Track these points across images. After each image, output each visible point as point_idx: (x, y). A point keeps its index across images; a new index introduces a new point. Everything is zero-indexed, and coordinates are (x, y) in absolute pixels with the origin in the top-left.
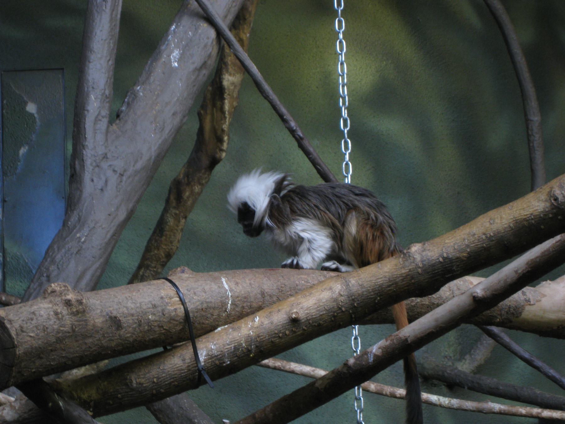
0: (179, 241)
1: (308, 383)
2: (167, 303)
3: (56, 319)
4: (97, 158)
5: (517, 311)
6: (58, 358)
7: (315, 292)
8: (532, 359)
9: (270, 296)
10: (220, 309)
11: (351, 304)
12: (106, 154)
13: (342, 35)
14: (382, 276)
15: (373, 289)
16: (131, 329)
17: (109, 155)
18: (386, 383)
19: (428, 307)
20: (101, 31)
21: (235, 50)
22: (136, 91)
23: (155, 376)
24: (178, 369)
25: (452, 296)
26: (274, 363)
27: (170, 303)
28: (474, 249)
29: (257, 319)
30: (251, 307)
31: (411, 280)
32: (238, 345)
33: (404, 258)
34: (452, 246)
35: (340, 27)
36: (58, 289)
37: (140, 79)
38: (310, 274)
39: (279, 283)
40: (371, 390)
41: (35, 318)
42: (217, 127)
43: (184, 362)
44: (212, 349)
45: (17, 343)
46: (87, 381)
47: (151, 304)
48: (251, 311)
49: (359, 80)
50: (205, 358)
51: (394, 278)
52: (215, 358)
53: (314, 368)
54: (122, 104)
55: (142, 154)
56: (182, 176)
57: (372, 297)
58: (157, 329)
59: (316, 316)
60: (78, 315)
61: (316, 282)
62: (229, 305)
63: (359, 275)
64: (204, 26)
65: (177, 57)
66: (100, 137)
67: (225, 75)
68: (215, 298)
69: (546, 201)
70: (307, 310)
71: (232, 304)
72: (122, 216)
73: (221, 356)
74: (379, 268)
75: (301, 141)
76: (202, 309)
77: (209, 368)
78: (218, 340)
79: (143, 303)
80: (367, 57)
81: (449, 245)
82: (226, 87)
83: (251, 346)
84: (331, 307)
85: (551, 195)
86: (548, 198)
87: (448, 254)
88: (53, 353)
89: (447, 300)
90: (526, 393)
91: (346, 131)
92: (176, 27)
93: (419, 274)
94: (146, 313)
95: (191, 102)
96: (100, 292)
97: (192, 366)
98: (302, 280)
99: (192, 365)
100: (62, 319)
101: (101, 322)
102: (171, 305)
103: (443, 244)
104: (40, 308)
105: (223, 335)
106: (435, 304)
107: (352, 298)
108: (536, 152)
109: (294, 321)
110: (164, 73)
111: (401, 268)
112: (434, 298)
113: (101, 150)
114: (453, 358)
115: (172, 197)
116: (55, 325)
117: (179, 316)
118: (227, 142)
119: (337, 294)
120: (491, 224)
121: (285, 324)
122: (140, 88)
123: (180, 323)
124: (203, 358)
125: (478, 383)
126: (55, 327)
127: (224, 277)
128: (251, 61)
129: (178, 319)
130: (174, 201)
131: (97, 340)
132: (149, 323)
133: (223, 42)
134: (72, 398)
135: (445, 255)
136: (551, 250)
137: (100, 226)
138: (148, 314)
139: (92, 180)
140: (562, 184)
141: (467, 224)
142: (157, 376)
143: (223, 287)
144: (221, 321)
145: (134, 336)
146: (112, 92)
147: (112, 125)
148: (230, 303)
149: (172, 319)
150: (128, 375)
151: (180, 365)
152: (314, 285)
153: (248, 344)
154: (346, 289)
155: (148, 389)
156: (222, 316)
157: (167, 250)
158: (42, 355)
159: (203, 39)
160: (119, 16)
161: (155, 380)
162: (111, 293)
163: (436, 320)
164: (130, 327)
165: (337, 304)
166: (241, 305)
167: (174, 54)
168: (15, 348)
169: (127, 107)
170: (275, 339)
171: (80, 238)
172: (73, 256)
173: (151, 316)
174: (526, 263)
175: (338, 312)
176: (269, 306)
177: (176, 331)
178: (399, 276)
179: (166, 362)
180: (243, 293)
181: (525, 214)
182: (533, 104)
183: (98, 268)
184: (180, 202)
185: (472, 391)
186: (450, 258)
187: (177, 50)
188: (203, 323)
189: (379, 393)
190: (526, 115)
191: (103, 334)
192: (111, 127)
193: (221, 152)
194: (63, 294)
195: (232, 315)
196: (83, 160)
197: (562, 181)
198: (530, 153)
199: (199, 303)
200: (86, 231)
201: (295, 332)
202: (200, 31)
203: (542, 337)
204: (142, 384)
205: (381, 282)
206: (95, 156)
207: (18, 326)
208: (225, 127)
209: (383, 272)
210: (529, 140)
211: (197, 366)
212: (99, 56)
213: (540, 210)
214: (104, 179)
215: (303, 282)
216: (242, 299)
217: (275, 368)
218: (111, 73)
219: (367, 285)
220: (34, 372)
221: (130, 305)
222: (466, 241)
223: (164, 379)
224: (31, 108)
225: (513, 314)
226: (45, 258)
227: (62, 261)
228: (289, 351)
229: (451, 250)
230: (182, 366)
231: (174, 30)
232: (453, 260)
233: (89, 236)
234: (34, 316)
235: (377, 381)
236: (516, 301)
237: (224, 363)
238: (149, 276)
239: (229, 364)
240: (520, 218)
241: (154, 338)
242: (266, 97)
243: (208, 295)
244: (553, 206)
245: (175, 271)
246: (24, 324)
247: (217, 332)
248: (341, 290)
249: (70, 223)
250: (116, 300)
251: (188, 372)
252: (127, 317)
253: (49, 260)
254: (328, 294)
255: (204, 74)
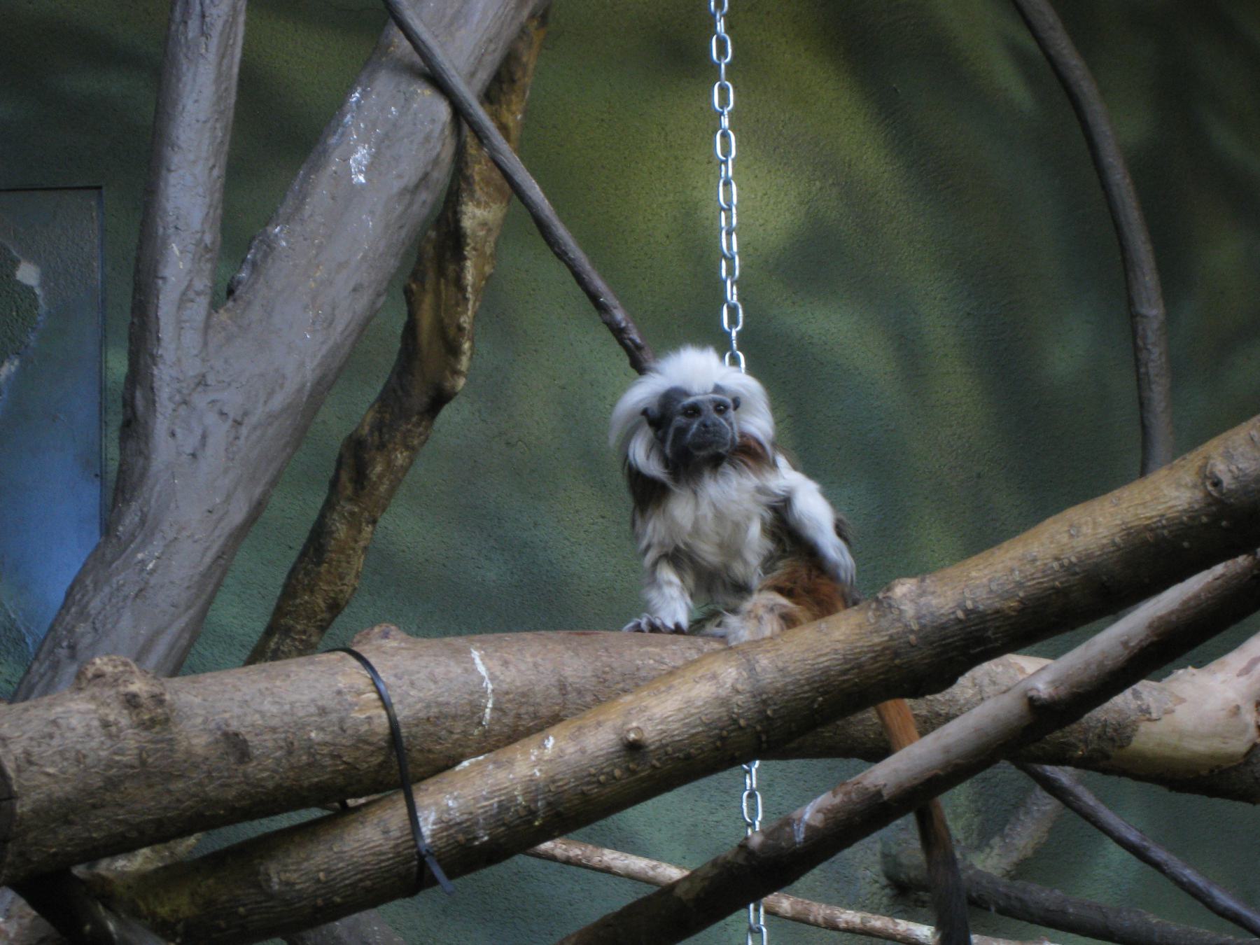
0: (357, 576)
1: (640, 896)
2: (350, 705)
3: (105, 735)
4: (184, 385)
5: (1120, 733)
6: (107, 823)
7: (680, 683)
8: (1145, 843)
9: (579, 692)
10: (467, 719)
11: (760, 712)
12: (204, 376)
13: (727, 120)
14: (828, 650)
15: (807, 679)
16: (270, 761)
17: (211, 379)
18: (815, 897)
19: (925, 722)
20: (196, 101)
21: (494, 150)
22: (272, 237)
23: (323, 867)
24: (372, 851)
25: (979, 697)
26: (566, 850)
27: (356, 705)
28: (1035, 592)
29: (550, 743)
30: (535, 716)
31: (892, 659)
32: (507, 799)
33: (877, 609)
34: (984, 586)
35: (724, 101)
36: (109, 669)
37: (281, 211)
38: (666, 645)
39: (599, 664)
40: (781, 911)
41: (57, 733)
42: (447, 321)
43: (386, 835)
44: (449, 809)
45: (19, 787)
46: (173, 875)
47: (316, 705)
48: (536, 725)
49: (761, 221)
50: (434, 827)
51: (855, 654)
52: (456, 828)
53: (655, 863)
54: (241, 267)
55: (284, 377)
56: (366, 429)
57: (806, 695)
58: (327, 761)
59: (680, 738)
60: (153, 727)
61: (680, 663)
62: (488, 711)
63: (777, 647)
64: (425, 93)
65: (365, 162)
66: (191, 339)
67: (467, 205)
68: (458, 694)
69: (1195, 486)
70: (661, 723)
71: (494, 709)
72: (238, 514)
73: (468, 824)
74: (821, 631)
75: (637, 353)
76: (428, 719)
77: (443, 850)
78: (463, 787)
79: (298, 704)
80: (778, 170)
81: (978, 582)
82: (469, 232)
83: (536, 801)
84: (716, 717)
85: (1205, 475)
86: (1199, 481)
87: (977, 602)
88: (99, 812)
89: (969, 706)
90: (1127, 924)
91: (734, 334)
92: (362, 96)
93: (913, 646)
94: (303, 726)
95: (392, 263)
96: (201, 677)
97: (404, 846)
98: (650, 658)
99: (403, 842)
100: (118, 737)
101: (203, 743)
102: (360, 710)
103: (965, 579)
104: (70, 712)
105: (473, 777)
106: (940, 715)
107: (762, 699)
108: (1153, 386)
109: (633, 748)
110: (333, 198)
111: (871, 632)
112: (939, 701)
113: (193, 368)
114: (963, 844)
115: (345, 476)
116: (104, 750)
117: (377, 734)
118: (468, 354)
119: (728, 688)
120: (1072, 536)
121: (612, 753)
122: (281, 230)
123: (381, 748)
124: (430, 827)
125: (1021, 900)
126: (103, 754)
127: (476, 649)
128: (528, 174)
129: (375, 739)
130: (348, 485)
131: (195, 784)
132: (310, 747)
133: (466, 128)
134: (135, 913)
135: (969, 605)
136: (1203, 597)
137: (188, 537)
138: (309, 728)
139: (173, 435)
140: (1231, 450)
141: (1017, 537)
142: (326, 866)
143: (475, 670)
144: (469, 747)
145: (277, 777)
146: (219, 239)
147: (217, 312)
148: (490, 705)
149: (361, 740)
150: (261, 864)
151: (378, 843)
152: (678, 668)
153: (529, 796)
154: (749, 678)
155: (305, 896)
156: (472, 735)
157: (332, 595)
158: (72, 817)
159: (422, 123)
160: (236, 70)
161: (322, 875)
162: (227, 681)
163: (947, 750)
164: (268, 757)
165: (727, 711)
166: (515, 712)
167: (358, 156)
168: (13, 801)
169: (252, 272)
170: (589, 788)
171: (143, 562)
172: (129, 602)
173: (315, 731)
174: (1147, 624)
175: (730, 728)
176: (577, 714)
177: (369, 767)
178: (866, 649)
179: (346, 836)
180: (519, 684)
181: (1148, 515)
182: (1148, 279)
183: (183, 630)
184: (363, 488)
185: (1007, 918)
186: (979, 612)
187: (364, 148)
188: (430, 751)
189: (799, 920)
190: (1130, 302)
191: (209, 773)
192: (216, 315)
193: (456, 377)
194: (120, 681)
195: (493, 733)
196: (152, 389)
197: (1230, 443)
198: (1139, 387)
199: (420, 704)
200: (157, 546)
201: (633, 772)
202: (415, 106)
203: (1174, 792)
204: (294, 884)
205: (826, 664)
206: (179, 380)
207: (20, 751)
208: (465, 320)
209: (831, 641)
210: (1137, 360)
211: (416, 846)
212: (191, 157)
213: (1180, 508)
214: (198, 433)
215: (651, 662)
216: (517, 697)
217: (568, 862)
218: (217, 195)
219: (795, 669)
220: (55, 854)
221: (268, 706)
222: (1017, 573)
223: (342, 874)
224: (28, 274)
225: (1112, 739)
226: (65, 607)
227: (103, 613)
228: (598, 823)
229: (982, 594)
230: (381, 845)
231: (358, 101)
232: (988, 615)
233: (164, 557)
234: (55, 728)
235: (796, 894)
236: (1120, 712)
237: (476, 838)
238: (290, 651)
239: (486, 842)
240: (1136, 523)
241: (320, 782)
242: (562, 255)
243: (440, 688)
244: (1210, 500)
245: (368, 634)
246: (33, 747)
247: (460, 771)
248: (737, 679)
249: (121, 528)
250: (238, 696)
251: (397, 859)
252: (261, 735)
253: (73, 610)
254: (707, 687)
255: (424, 202)
